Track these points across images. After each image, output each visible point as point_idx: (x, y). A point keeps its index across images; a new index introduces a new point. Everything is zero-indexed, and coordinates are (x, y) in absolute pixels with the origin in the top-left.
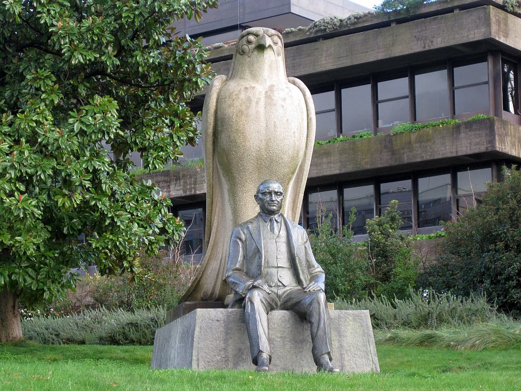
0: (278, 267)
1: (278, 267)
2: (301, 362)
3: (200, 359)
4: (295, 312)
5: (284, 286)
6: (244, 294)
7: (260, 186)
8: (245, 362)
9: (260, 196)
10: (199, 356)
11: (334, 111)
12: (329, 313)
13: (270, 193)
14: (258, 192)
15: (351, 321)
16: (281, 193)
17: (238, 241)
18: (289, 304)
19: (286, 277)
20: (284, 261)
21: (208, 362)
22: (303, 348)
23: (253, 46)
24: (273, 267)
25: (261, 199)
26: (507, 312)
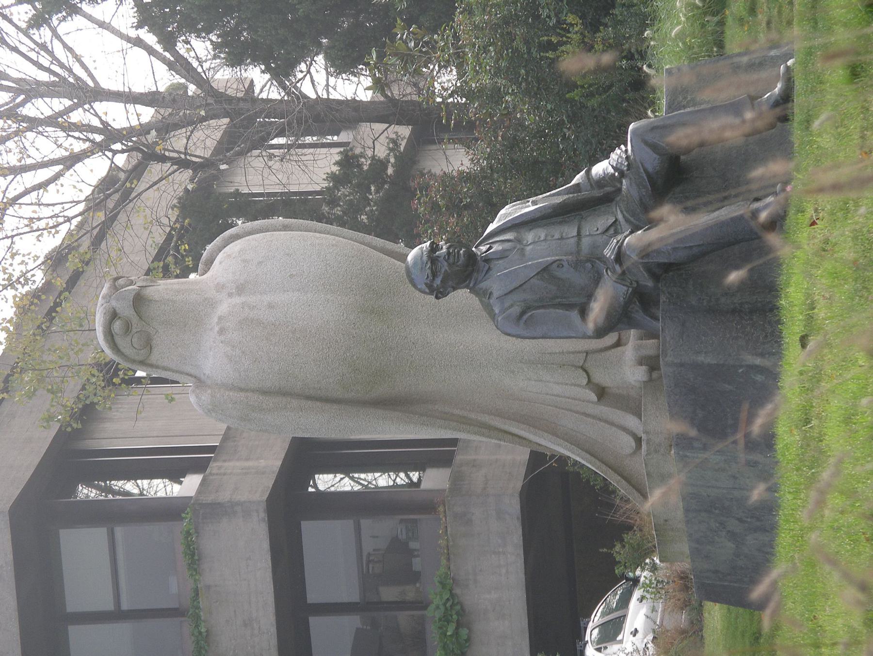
5: (616, 220)
6: (631, 284)
15: (685, 98)
17: (525, 317)
21: (766, 336)
23: (135, 320)
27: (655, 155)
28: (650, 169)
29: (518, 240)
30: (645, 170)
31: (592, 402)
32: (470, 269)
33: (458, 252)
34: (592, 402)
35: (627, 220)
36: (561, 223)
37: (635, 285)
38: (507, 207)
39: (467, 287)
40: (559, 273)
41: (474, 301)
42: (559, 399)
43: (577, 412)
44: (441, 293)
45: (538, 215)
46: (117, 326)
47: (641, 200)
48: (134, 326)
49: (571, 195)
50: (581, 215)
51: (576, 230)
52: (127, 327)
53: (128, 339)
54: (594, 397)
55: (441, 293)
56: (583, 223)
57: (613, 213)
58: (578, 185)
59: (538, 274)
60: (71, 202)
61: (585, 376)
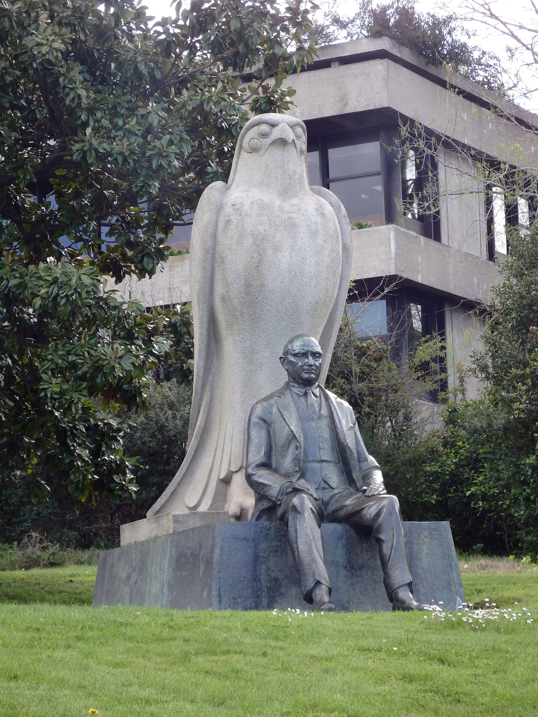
0: (322, 461)
1: (322, 461)
2: (361, 597)
3: (222, 594)
4: (350, 526)
5: (333, 489)
6: (279, 500)
7: (257, 403)
8: (284, 598)
9: (292, 359)
10: (221, 589)
11: (379, 174)
12: (395, 533)
13: (305, 355)
14: (286, 353)
15: (426, 537)
16: (320, 354)
18: (342, 513)
19: (334, 477)
20: (327, 454)
21: (234, 598)
22: (362, 577)
23: (269, 140)
24: (314, 461)
25: (291, 362)
26: (471, 301)
27: (373, 515)
28: (364, 512)
29: (320, 417)
30: (363, 509)
31: (219, 475)
32: (300, 381)
33: (312, 373)
34: (219, 475)
35: (333, 497)
36: (333, 448)
37: (279, 503)
38: (351, 407)
39: (289, 380)
40: (292, 447)
41: (282, 384)
42: (214, 449)
43: (213, 464)
44: (284, 361)
45: (339, 431)
46: (264, 128)
47: (345, 506)
48: (265, 140)
49: (356, 455)
50: (339, 463)
51: (329, 459)
52: (264, 135)
53: (256, 136)
54: (222, 476)
55: (284, 361)
56: (332, 464)
57: (340, 486)
58: (366, 460)
59: (292, 431)
60: (510, 32)
61: (237, 469)
